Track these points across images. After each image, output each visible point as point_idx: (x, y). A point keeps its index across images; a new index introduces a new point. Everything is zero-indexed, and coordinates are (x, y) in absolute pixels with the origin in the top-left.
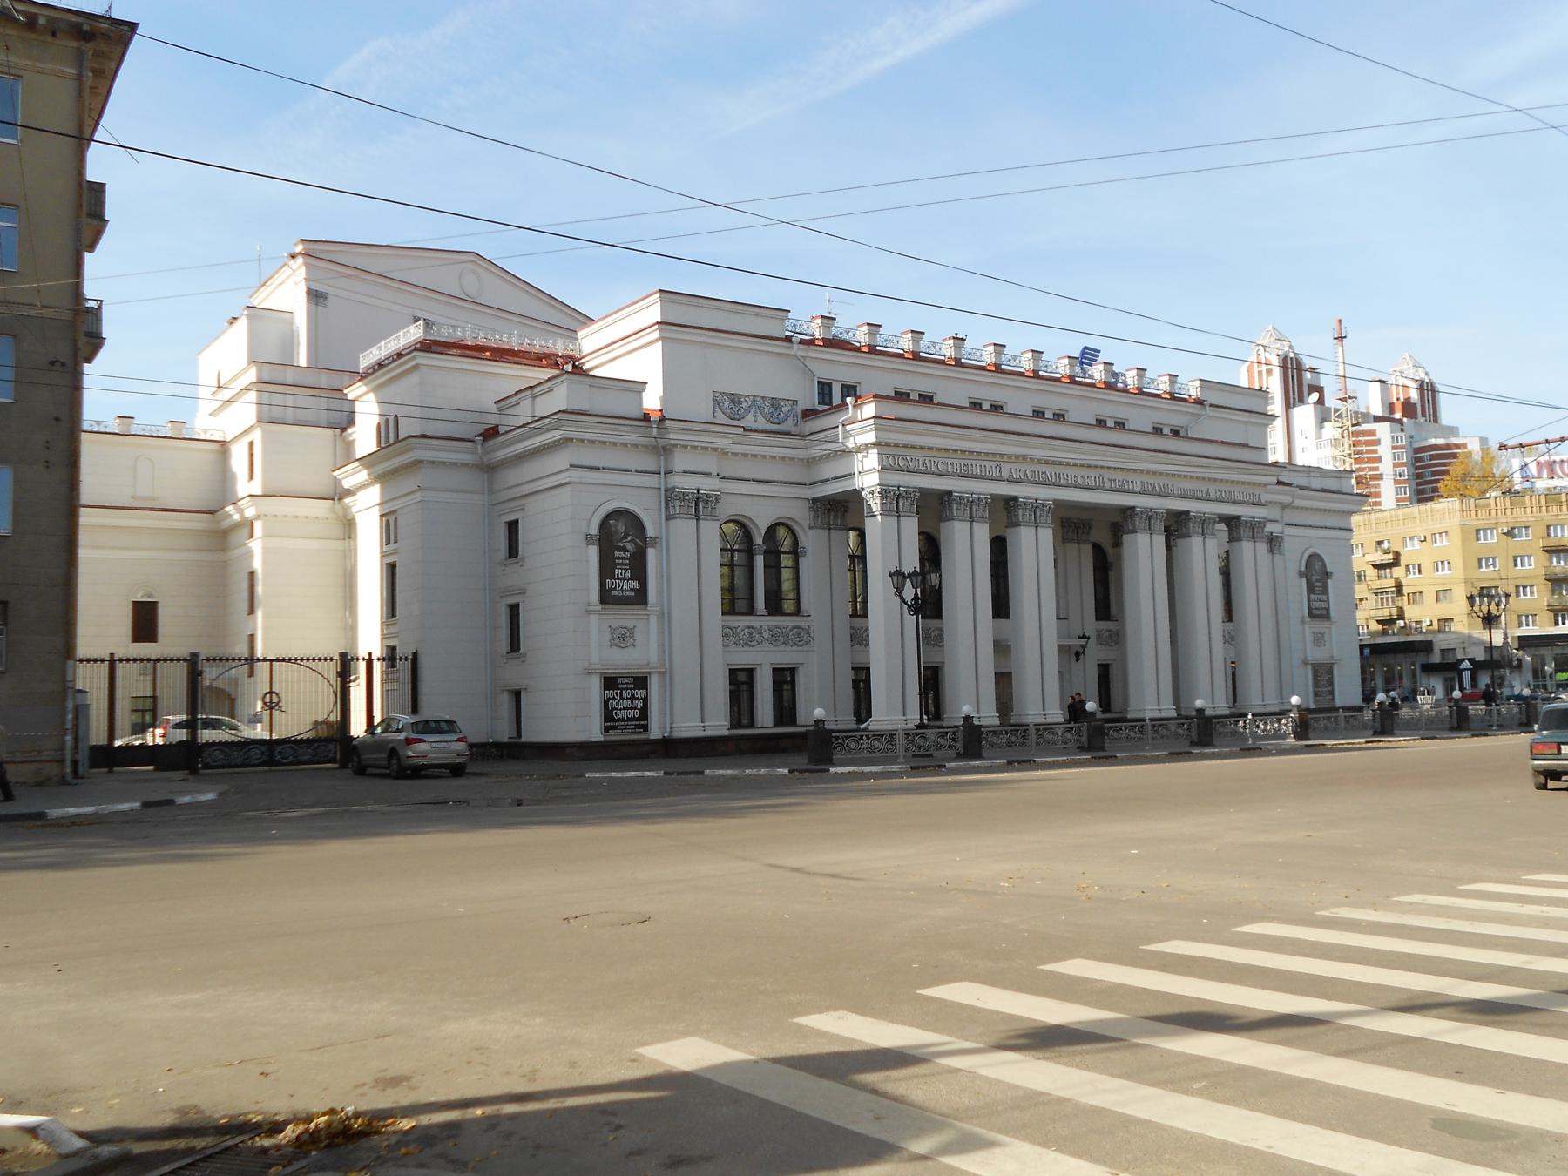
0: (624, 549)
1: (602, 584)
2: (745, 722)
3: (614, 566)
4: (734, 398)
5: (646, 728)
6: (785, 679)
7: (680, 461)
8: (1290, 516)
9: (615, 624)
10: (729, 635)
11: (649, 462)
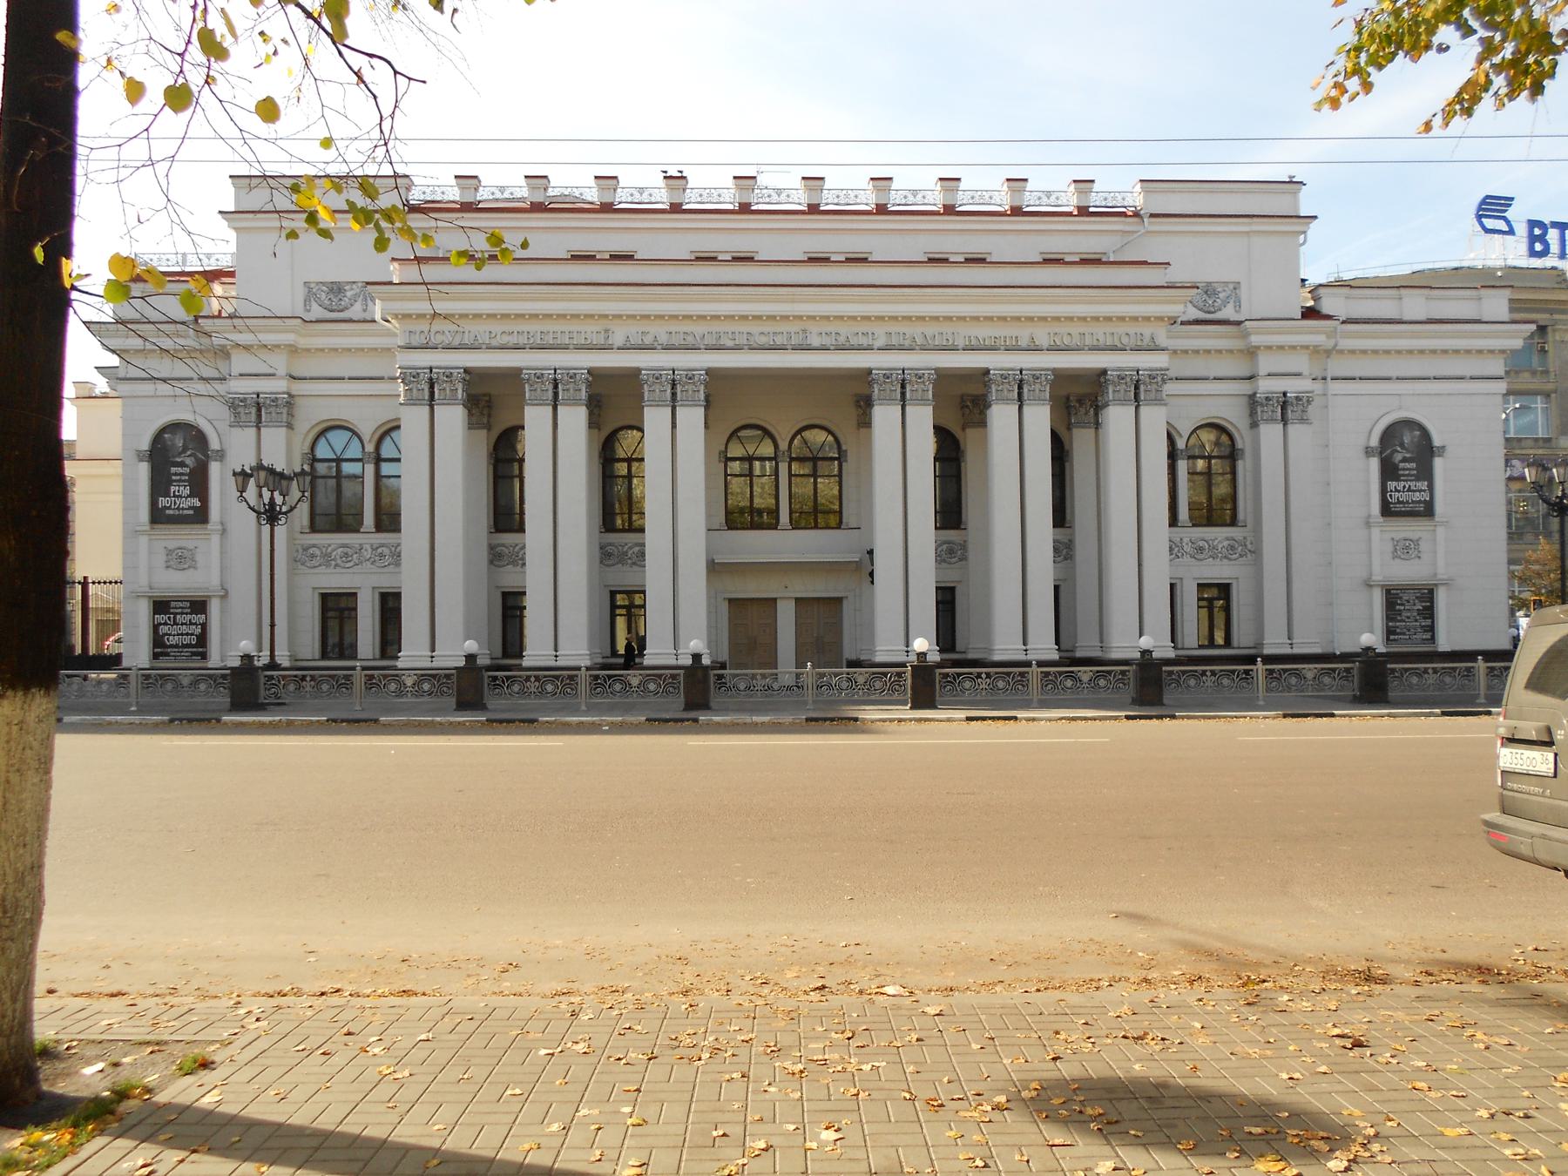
2: (1219, 640)
3: (170, 483)
4: (336, 289)
5: (204, 656)
6: (390, 605)
7: (1265, 364)
8: (1337, 366)
9: (172, 545)
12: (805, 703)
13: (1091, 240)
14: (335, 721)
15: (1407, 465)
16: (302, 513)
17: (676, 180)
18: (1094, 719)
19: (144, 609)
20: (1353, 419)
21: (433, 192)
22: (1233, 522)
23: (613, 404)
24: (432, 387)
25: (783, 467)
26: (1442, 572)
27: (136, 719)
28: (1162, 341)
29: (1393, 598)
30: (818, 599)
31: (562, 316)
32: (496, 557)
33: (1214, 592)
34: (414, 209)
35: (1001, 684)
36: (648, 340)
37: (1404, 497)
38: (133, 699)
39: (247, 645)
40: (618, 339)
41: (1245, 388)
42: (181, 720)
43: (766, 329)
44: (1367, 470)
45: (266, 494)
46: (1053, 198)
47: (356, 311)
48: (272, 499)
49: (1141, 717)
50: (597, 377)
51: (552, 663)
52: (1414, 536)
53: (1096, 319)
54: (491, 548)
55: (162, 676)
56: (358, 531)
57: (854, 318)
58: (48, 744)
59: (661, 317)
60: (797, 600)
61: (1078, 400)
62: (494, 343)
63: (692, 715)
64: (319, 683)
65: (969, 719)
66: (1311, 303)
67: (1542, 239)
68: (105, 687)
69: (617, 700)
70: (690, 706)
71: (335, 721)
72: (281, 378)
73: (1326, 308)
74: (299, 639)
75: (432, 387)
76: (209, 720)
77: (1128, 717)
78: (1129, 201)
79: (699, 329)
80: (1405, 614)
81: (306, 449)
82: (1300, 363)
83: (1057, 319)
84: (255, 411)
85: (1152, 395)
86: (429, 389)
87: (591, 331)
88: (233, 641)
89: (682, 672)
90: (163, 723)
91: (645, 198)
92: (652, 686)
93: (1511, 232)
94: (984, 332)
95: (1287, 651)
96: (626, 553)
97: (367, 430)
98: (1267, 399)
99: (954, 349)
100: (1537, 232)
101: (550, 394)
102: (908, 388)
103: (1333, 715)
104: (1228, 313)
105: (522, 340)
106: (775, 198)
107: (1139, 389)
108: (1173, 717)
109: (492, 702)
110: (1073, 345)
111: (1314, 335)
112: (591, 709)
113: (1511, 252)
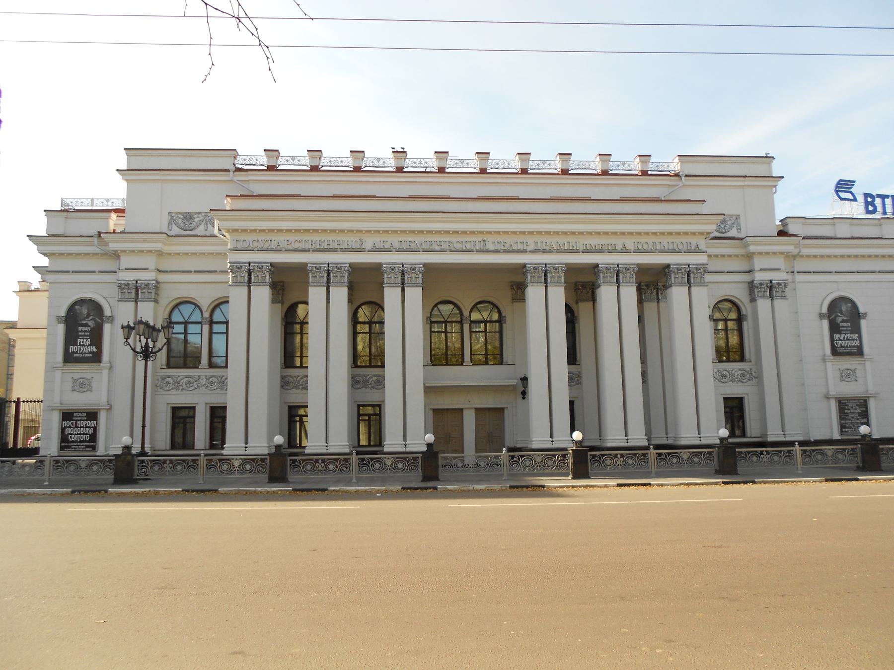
0: (86, 325)
1: (66, 350)
3: (78, 337)
4: (188, 217)
5: (94, 448)
6: (218, 414)
7: (758, 263)
8: (799, 265)
9: (77, 376)
10: (721, 378)
11: (109, 265)
12: (503, 475)
13: (659, 188)
14: (187, 491)
15: (845, 324)
16: (162, 356)
17: (400, 154)
18: (702, 484)
19: (56, 417)
20: (812, 295)
21: (251, 160)
22: (742, 359)
23: (365, 288)
24: (250, 275)
25: (466, 327)
26: (871, 389)
27: (48, 491)
28: (703, 247)
29: (843, 405)
30: (489, 409)
31: (333, 231)
32: (285, 383)
33: (735, 404)
34: (238, 170)
35: (630, 461)
36: (387, 246)
37: (844, 343)
38: (46, 477)
39: (126, 440)
40: (368, 245)
41: (746, 278)
42: (80, 491)
43: (460, 240)
44: (822, 328)
45: (144, 341)
46: (626, 165)
47: (201, 230)
48: (147, 343)
49: (733, 483)
50: (355, 269)
51: (325, 451)
52: (853, 367)
53: (663, 234)
54: (283, 378)
55: (67, 461)
56: (197, 367)
57: (515, 233)
58: (44, 396)
59: (396, 232)
60: (476, 409)
61: (652, 283)
62: (290, 247)
63: (430, 484)
64: (175, 466)
65: (619, 485)
66: (781, 228)
67: (872, 204)
68: (27, 469)
69: (376, 475)
70: (426, 479)
71: (187, 491)
72: (152, 271)
73: (791, 229)
74: (160, 437)
75: (250, 275)
76: (99, 491)
77: (724, 483)
78: (671, 168)
79: (419, 239)
80: (851, 415)
81: (166, 316)
82: (779, 262)
83: (639, 234)
84: (135, 291)
85: (699, 280)
86: (248, 276)
87: (351, 240)
88: (114, 438)
89: (420, 455)
90: (67, 493)
91: (381, 164)
92: (400, 465)
93: (855, 200)
94: (595, 242)
95: (782, 439)
96: (367, 381)
97: (205, 303)
98: (761, 284)
99: (577, 251)
100: (869, 200)
101: (325, 279)
102: (549, 275)
103: (857, 480)
104: (733, 233)
105: (308, 246)
106: (460, 164)
107: (690, 276)
108: (754, 482)
109: (291, 477)
110: (649, 249)
111: (785, 245)
112: (359, 482)
113: (857, 210)
